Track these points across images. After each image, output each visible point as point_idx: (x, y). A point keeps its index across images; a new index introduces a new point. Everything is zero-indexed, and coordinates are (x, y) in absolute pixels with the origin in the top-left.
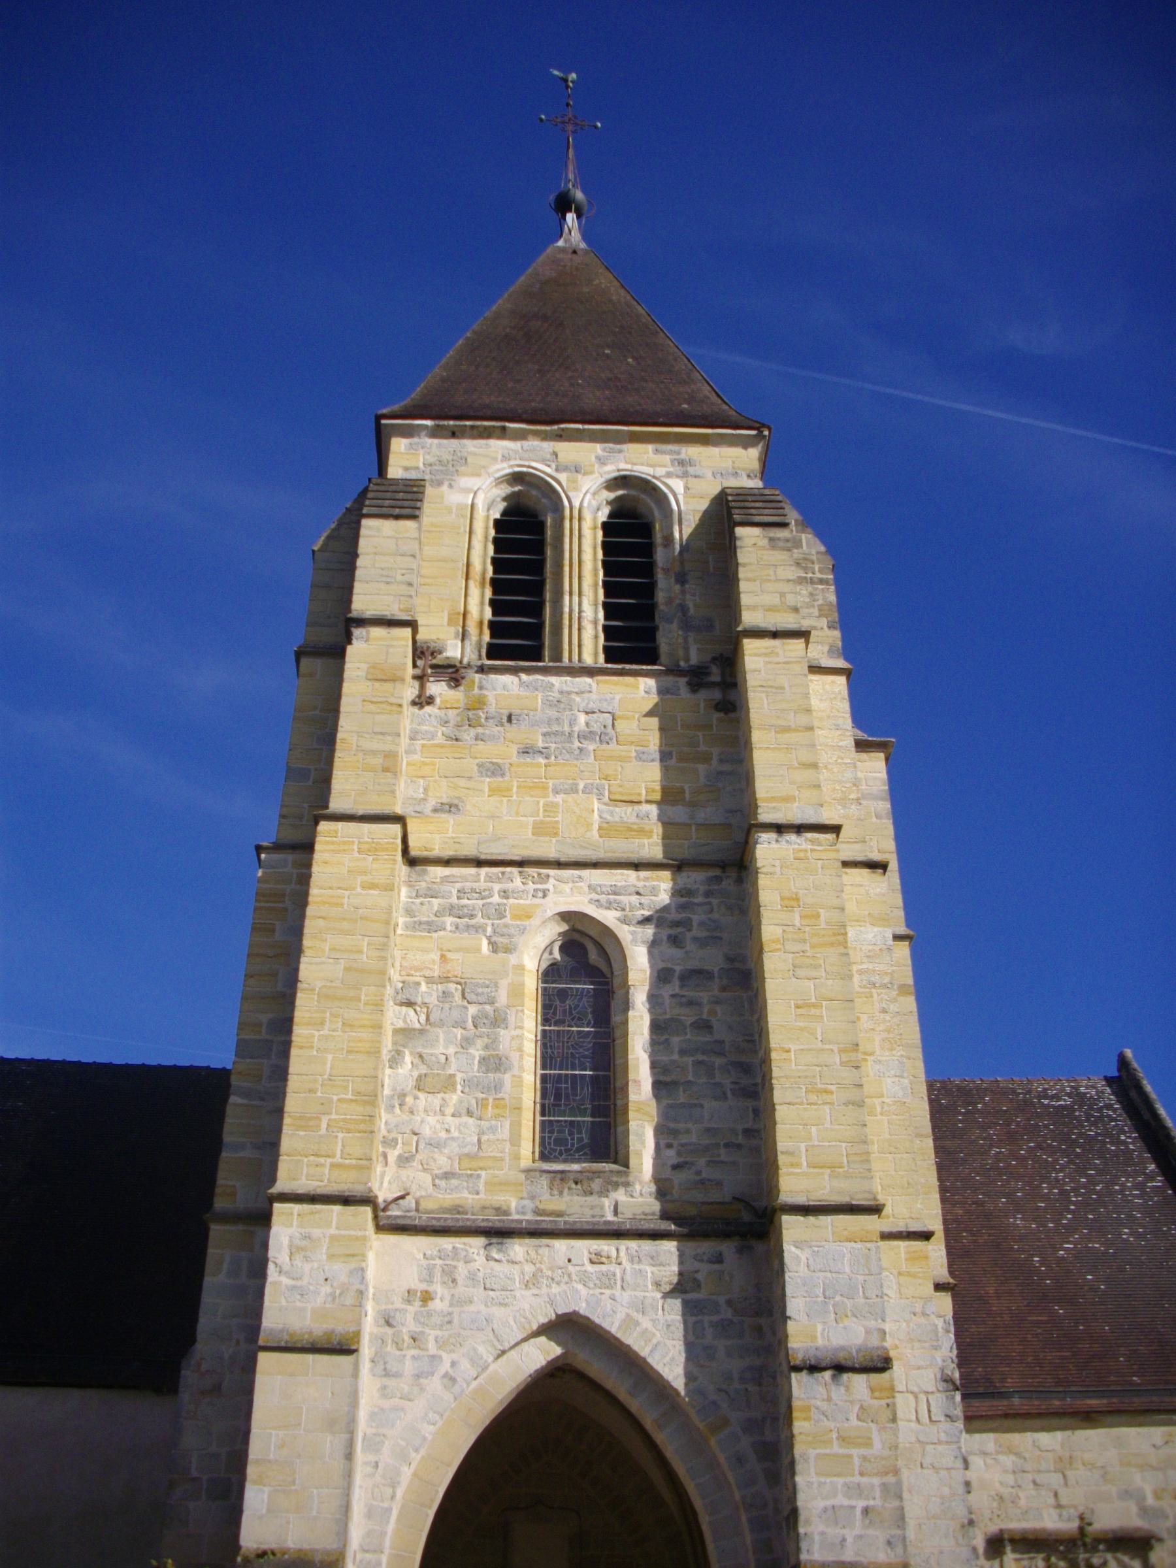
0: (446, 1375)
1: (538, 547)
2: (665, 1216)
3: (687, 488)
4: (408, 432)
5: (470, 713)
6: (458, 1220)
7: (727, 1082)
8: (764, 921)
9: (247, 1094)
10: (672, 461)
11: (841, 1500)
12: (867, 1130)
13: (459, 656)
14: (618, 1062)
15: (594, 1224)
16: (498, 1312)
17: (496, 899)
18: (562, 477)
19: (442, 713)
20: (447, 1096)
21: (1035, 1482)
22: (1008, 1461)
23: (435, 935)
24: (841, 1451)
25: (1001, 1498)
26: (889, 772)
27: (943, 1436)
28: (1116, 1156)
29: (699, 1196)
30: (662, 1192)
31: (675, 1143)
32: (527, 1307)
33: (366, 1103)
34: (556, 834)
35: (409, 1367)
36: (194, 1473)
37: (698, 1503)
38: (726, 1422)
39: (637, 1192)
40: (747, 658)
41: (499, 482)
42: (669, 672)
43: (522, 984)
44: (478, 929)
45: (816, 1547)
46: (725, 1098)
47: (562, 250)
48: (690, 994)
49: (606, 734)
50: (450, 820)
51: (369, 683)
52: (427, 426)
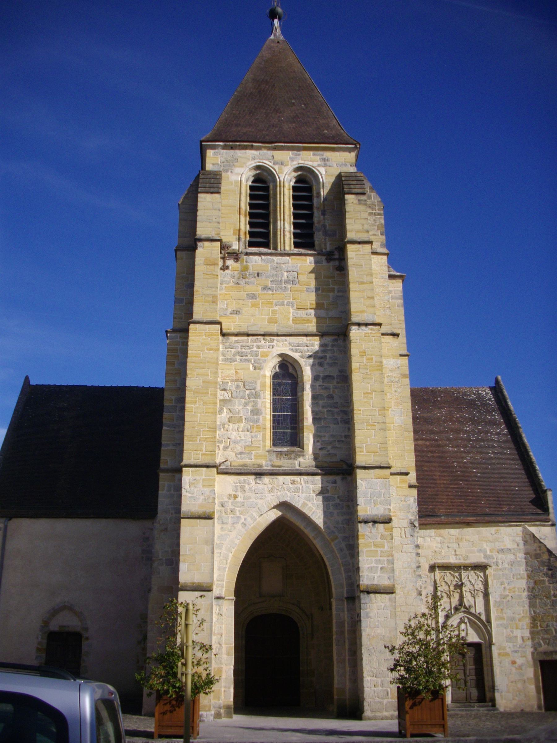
0: (243, 523)
1: (266, 198)
2: (317, 467)
3: (326, 172)
4: (213, 148)
6: (245, 469)
7: (339, 418)
8: (353, 361)
9: (169, 426)
10: (320, 159)
11: (374, 565)
12: (387, 439)
13: (238, 248)
14: (300, 410)
15: (292, 470)
16: (260, 501)
17: (255, 349)
18: (276, 167)
19: (232, 273)
21: (448, 547)
22: (439, 539)
24: (374, 549)
26: (403, 287)
27: (409, 542)
30: (315, 459)
31: (320, 441)
32: (269, 499)
33: (212, 431)
34: (276, 322)
35: (230, 521)
36: (160, 557)
37: (327, 563)
39: (307, 458)
40: (348, 253)
41: (251, 169)
42: (318, 254)
43: (265, 382)
44: (249, 361)
45: (365, 579)
47: (273, 41)
50: (237, 317)
51: (205, 266)
52: (220, 145)
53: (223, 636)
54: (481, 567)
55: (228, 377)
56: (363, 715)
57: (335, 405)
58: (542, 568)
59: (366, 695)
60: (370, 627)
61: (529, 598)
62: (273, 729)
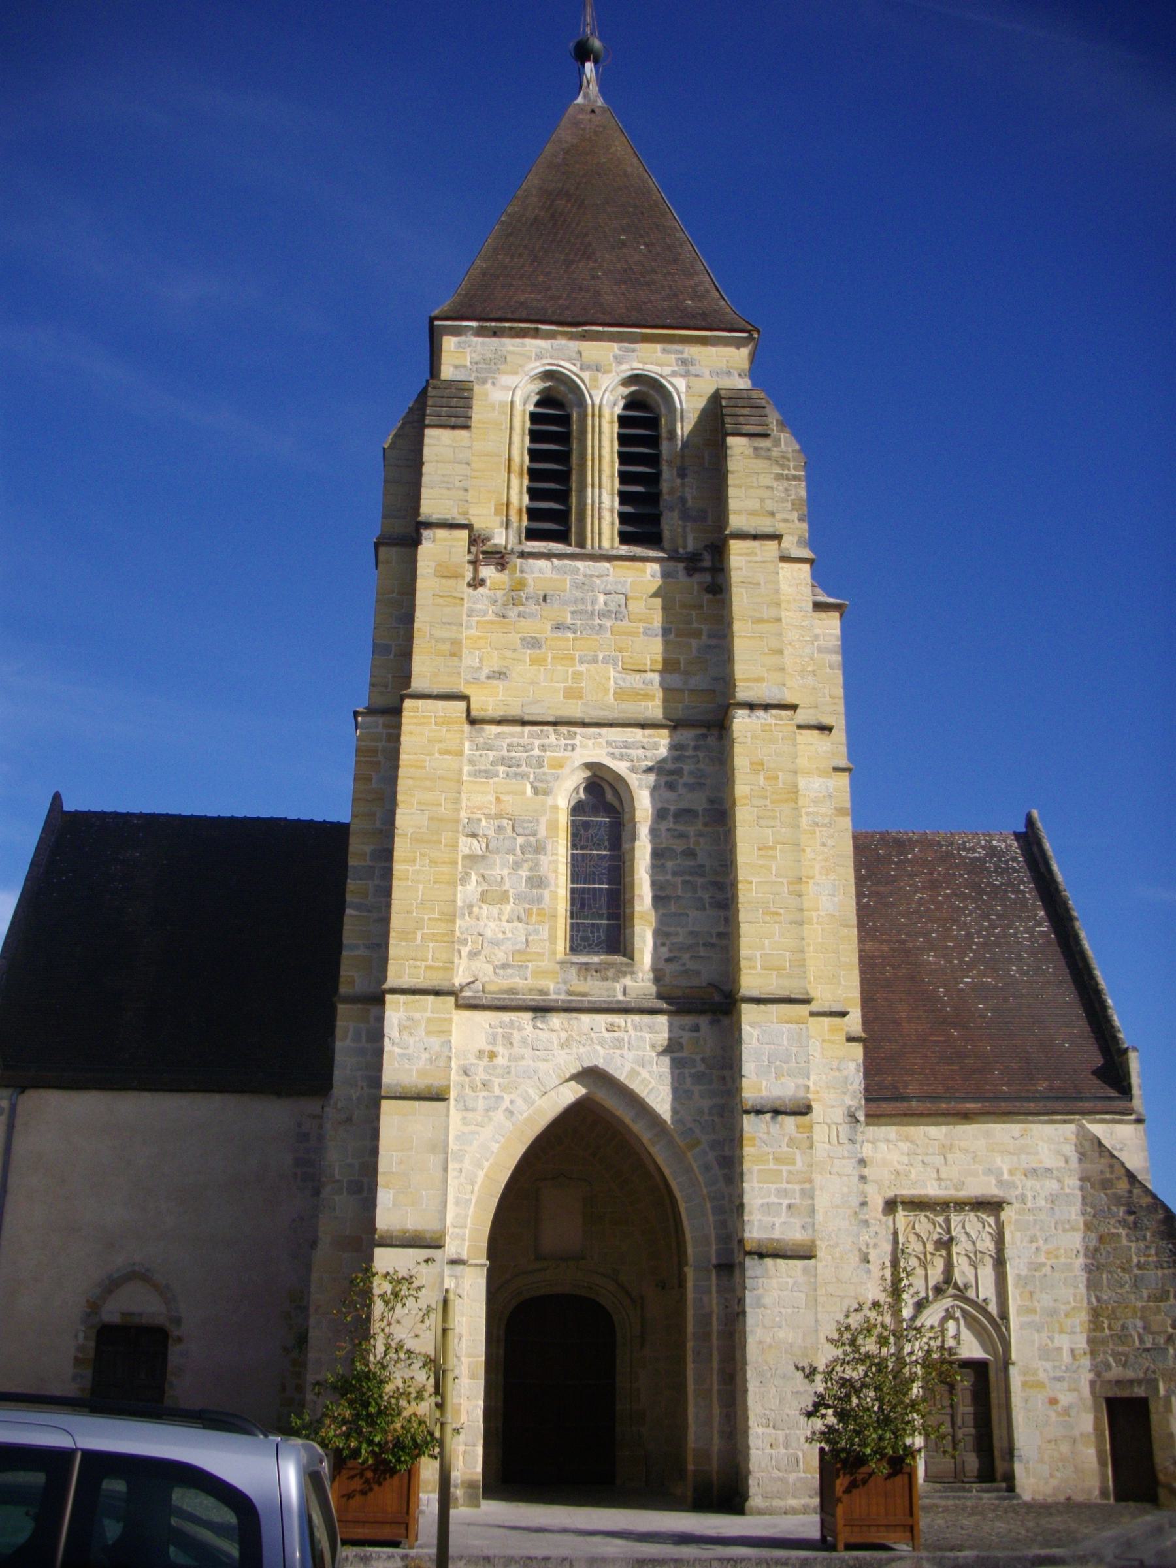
0: (507, 1109)
1: (564, 438)
2: (660, 996)
3: (688, 387)
4: (457, 332)
5: (514, 594)
6: (512, 999)
7: (706, 897)
9: (357, 907)
10: (677, 360)
12: (804, 943)
14: (627, 879)
15: (609, 1002)
16: (542, 1066)
17: (536, 752)
18: (586, 375)
20: (502, 907)
21: (923, 1162)
22: (905, 1146)
23: (491, 781)
25: (898, 1173)
28: (1015, 903)
29: (684, 982)
30: (658, 979)
31: (668, 942)
32: (562, 1062)
33: (448, 920)
35: (481, 1104)
36: (337, 1177)
37: (678, 1195)
38: (698, 1142)
39: (640, 977)
40: (732, 558)
41: (533, 378)
42: (670, 558)
43: (557, 821)
44: (524, 776)
45: (755, 1229)
46: (705, 909)
47: (581, 108)
48: (681, 828)
49: (620, 612)
50: (500, 685)
51: (437, 579)
53: (464, 1339)
54: (991, 1206)
55: (479, 809)
56: (747, 1504)
57: (699, 871)
58: (1114, 1208)
59: (753, 1465)
60: (764, 1327)
61: (1088, 1269)
62: (565, 1531)
